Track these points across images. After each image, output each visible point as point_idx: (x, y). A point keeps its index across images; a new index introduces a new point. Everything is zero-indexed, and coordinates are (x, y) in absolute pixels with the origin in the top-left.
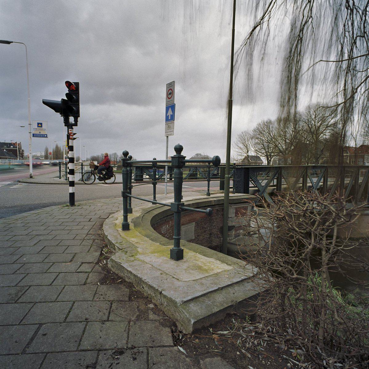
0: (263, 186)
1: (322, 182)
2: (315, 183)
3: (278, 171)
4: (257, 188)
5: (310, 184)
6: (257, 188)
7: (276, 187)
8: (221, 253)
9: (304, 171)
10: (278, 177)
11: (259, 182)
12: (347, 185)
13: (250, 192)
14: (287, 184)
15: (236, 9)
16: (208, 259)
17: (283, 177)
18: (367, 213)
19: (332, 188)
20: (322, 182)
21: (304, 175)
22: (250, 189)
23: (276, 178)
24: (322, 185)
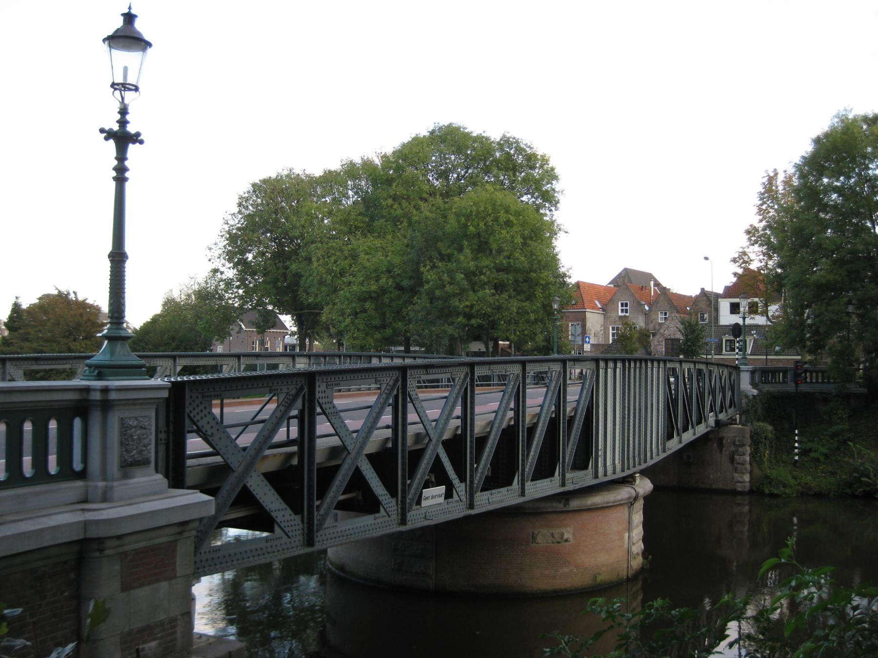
0: (244, 449)
1: (458, 417)
2: (434, 424)
3: (302, 388)
4: (218, 459)
5: (419, 428)
6: (218, 459)
7: (295, 448)
8: (12, 311)
9: (394, 385)
10: (302, 412)
11: (228, 437)
12: (573, 414)
13: (189, 480)
14: (337, 434)
15: (40, 400)
16: (15, 611)
17: (318, 410)
18: (594, 504)
19: (489, 433)
20: (458, 417)
21: (396, 397)
22: (189, 462)
23: (294, 412)
24: (387, 439)
